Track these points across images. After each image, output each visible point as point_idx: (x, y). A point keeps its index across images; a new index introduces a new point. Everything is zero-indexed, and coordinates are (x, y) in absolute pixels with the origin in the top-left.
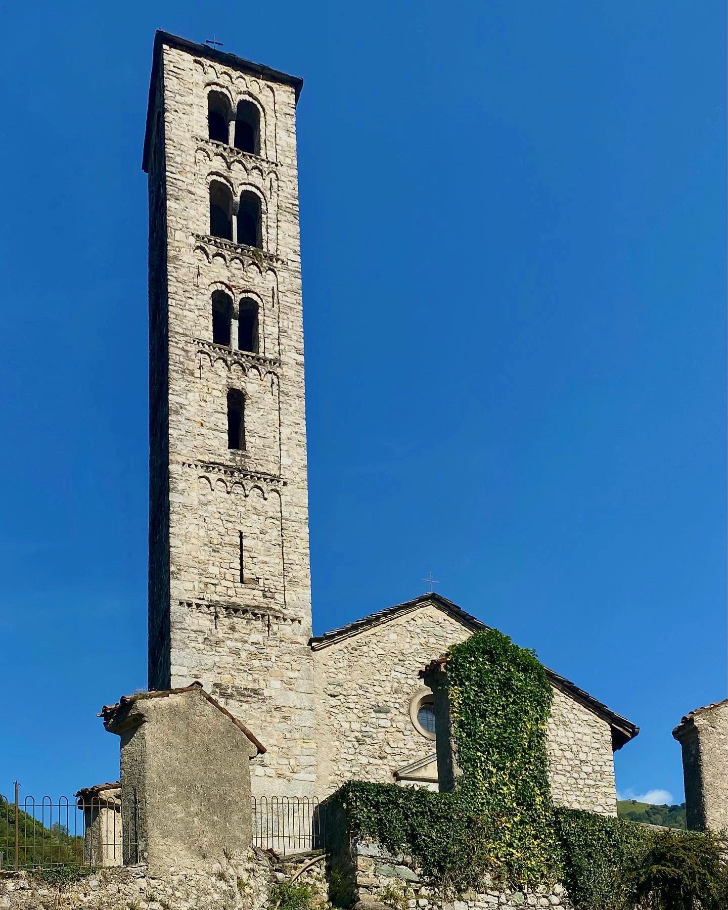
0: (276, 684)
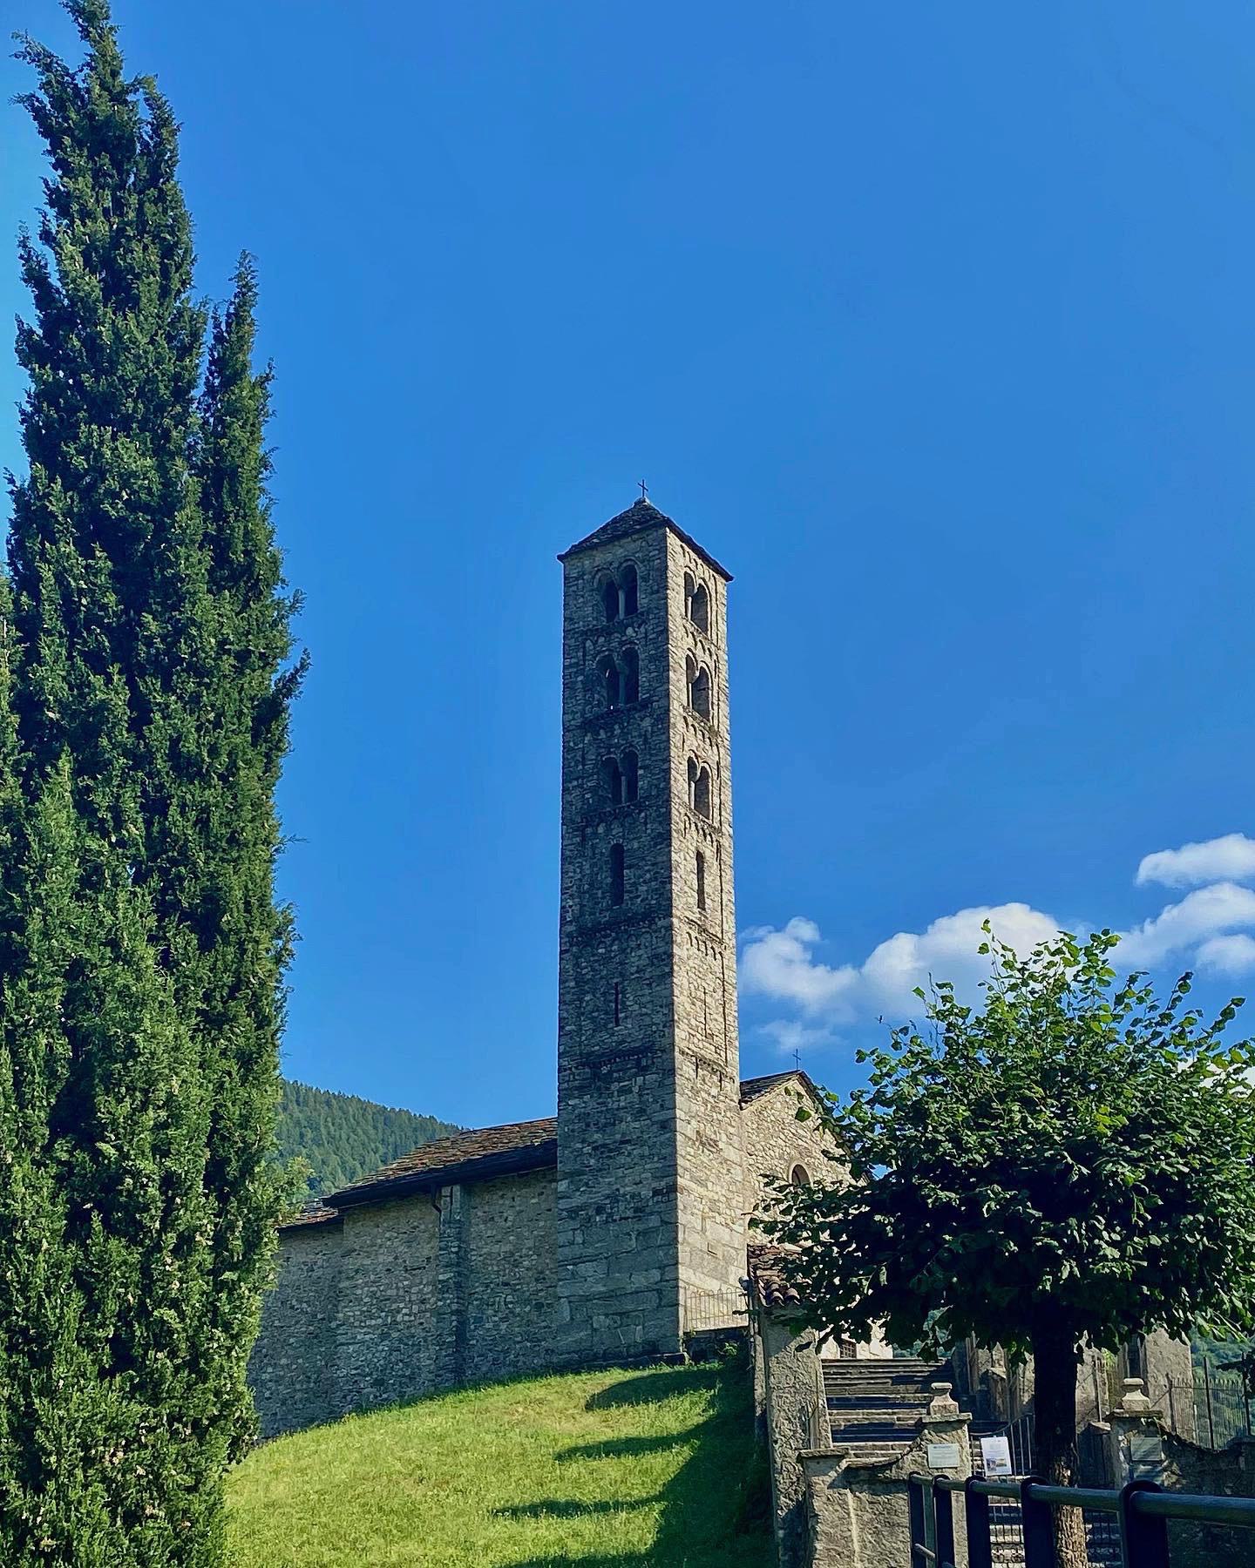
0: (724, 1138)
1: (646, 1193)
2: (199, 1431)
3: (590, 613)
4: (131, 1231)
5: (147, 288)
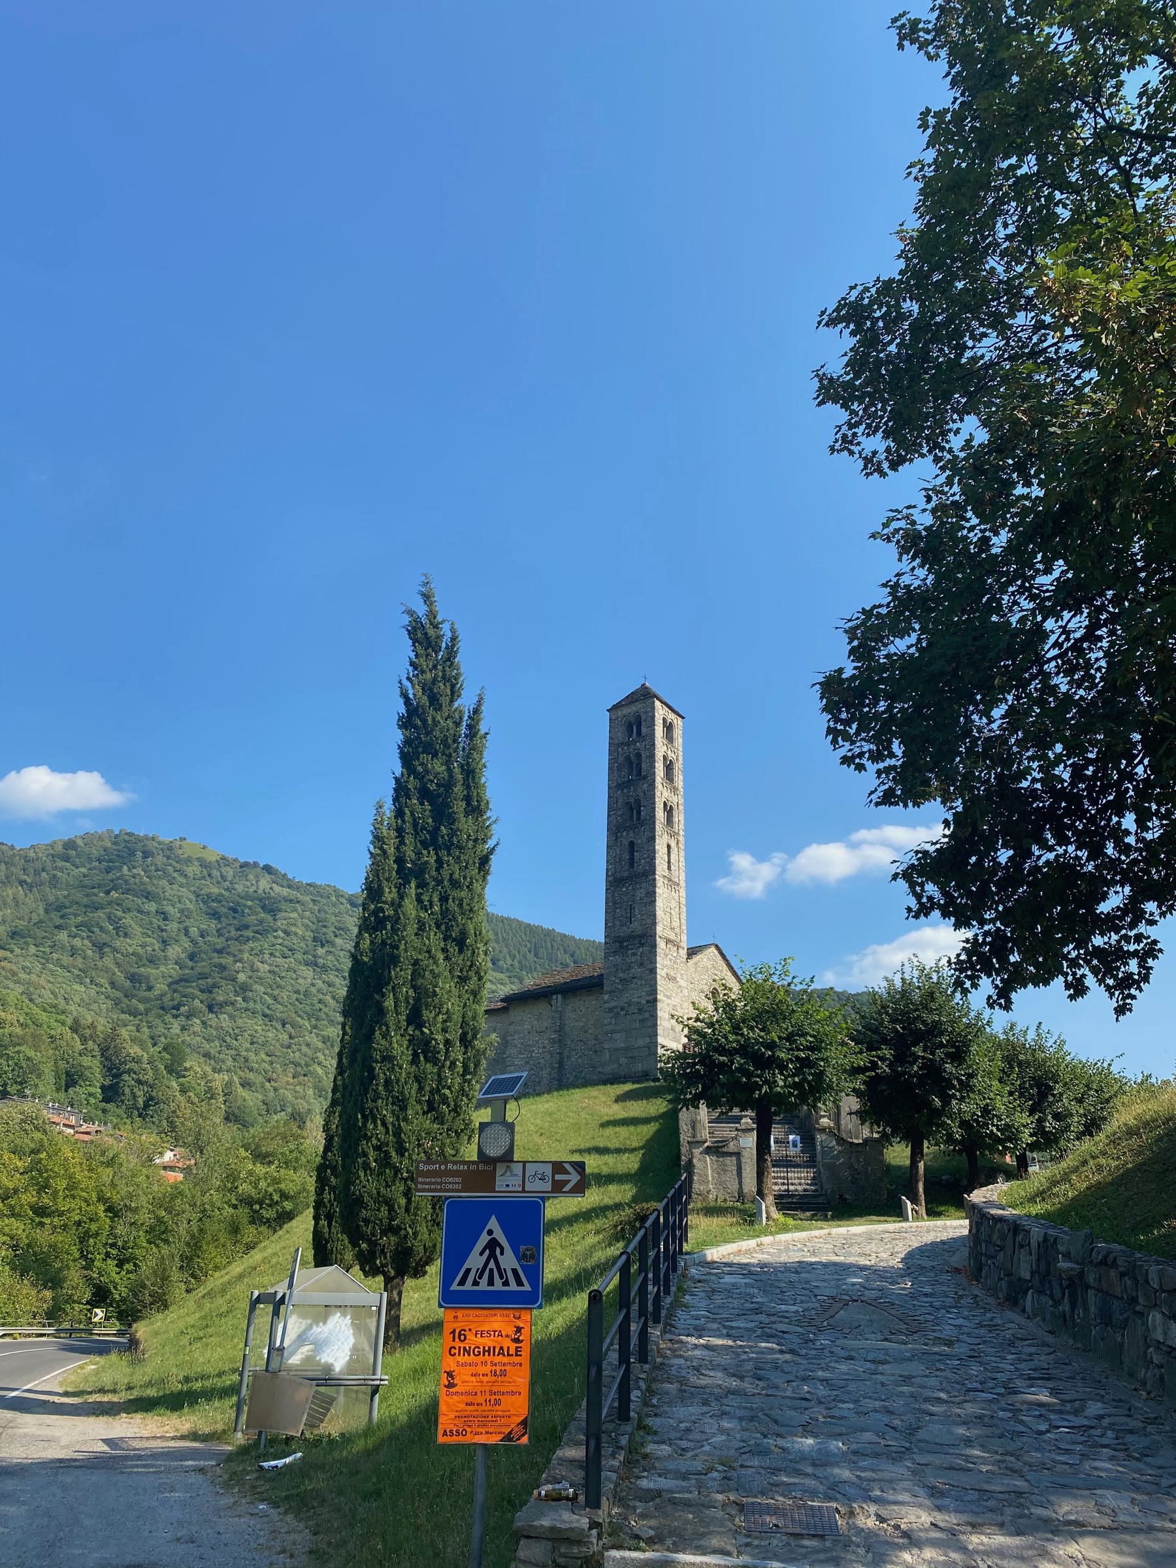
1: (643, 1002)
2: (458, 1134)
3: (621, 736)
4: (435, 1062)
5: (444, 700)
